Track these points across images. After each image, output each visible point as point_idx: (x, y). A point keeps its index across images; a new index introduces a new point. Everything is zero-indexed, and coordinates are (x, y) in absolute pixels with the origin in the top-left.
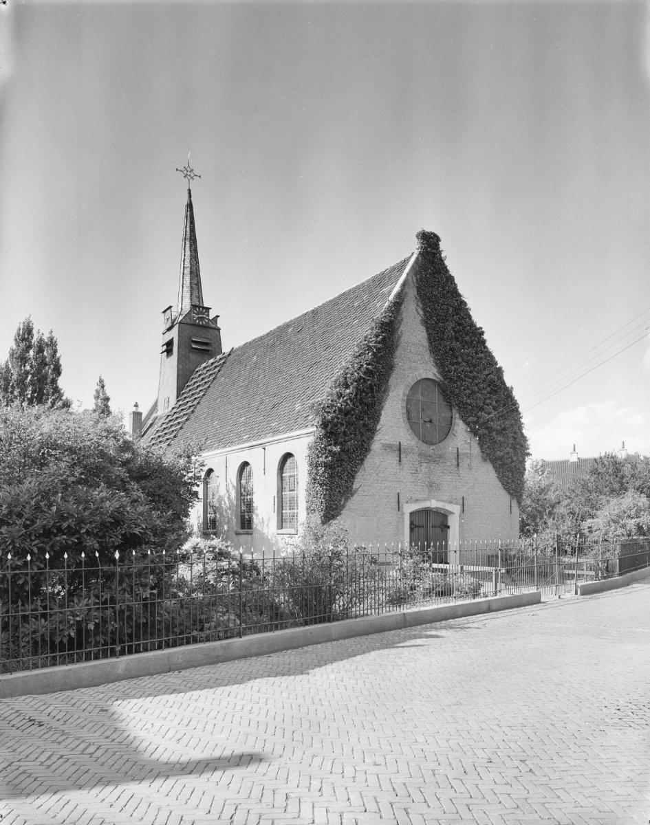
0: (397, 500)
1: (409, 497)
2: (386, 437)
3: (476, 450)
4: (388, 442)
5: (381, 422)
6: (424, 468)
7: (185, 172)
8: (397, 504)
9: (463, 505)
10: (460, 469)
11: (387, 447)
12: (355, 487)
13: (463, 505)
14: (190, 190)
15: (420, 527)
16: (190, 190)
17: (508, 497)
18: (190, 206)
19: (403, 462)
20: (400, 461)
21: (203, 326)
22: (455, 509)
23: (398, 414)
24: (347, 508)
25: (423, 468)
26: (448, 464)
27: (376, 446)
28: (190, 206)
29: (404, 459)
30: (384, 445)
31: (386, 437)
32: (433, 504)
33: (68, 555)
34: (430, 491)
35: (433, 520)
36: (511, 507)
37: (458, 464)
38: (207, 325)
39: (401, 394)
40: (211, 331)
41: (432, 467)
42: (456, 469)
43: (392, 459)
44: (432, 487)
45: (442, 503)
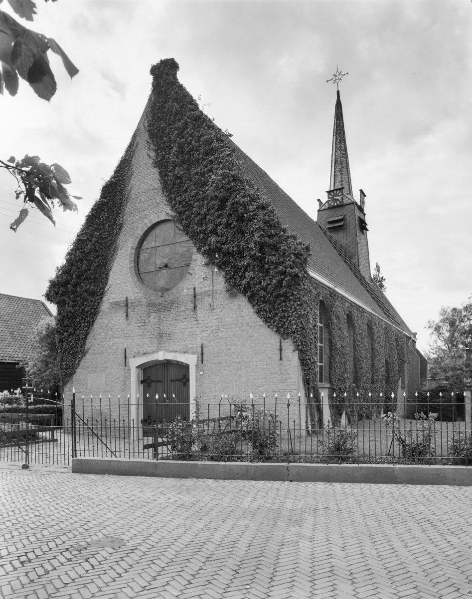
0: (124, 356)
1: (137, 352)
2: (114, 296)
3: (220, 282)
4: (115, 300)
5: (110, 282)
6: (153, 318)
7: (338, 74)
8: (124, 359)
9: (202, 354)
10: (199, 311)
11: (115, 305)
12: (86, 347)
13: (202, 354)
14: (338, 92)
15: (157, 382)
16: (338, 92)
17: (274, 339)
18: (339, 105)
19: (130, 316)
20: (127, 316)
21: (338, 206)
22: (135, 362)
23: (125, 269)
24: (81, 366)
25: (151, 319)
26: (183, 308)
27: (105, 306)
28: (339, 105)
29: (131, 313)
30: (111, 304)
31: (114, 296)
32: (161, 356)
33: (159, 396)
34: (160, 343)
35: (173, 373)
36: (281, 350)
37: (195, 308)
38: (341, 204)
39: (129, 249)
40: (347, 207)
41: (162, 316)
42: (193, 313)
43: (120, 316)
44: (162, 337)
45: (173, 354)
